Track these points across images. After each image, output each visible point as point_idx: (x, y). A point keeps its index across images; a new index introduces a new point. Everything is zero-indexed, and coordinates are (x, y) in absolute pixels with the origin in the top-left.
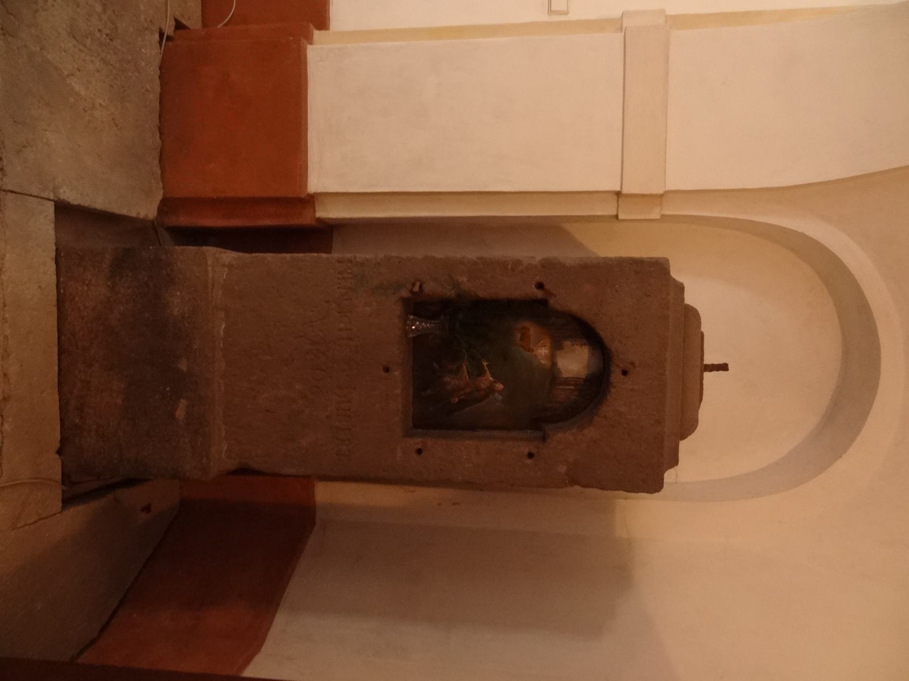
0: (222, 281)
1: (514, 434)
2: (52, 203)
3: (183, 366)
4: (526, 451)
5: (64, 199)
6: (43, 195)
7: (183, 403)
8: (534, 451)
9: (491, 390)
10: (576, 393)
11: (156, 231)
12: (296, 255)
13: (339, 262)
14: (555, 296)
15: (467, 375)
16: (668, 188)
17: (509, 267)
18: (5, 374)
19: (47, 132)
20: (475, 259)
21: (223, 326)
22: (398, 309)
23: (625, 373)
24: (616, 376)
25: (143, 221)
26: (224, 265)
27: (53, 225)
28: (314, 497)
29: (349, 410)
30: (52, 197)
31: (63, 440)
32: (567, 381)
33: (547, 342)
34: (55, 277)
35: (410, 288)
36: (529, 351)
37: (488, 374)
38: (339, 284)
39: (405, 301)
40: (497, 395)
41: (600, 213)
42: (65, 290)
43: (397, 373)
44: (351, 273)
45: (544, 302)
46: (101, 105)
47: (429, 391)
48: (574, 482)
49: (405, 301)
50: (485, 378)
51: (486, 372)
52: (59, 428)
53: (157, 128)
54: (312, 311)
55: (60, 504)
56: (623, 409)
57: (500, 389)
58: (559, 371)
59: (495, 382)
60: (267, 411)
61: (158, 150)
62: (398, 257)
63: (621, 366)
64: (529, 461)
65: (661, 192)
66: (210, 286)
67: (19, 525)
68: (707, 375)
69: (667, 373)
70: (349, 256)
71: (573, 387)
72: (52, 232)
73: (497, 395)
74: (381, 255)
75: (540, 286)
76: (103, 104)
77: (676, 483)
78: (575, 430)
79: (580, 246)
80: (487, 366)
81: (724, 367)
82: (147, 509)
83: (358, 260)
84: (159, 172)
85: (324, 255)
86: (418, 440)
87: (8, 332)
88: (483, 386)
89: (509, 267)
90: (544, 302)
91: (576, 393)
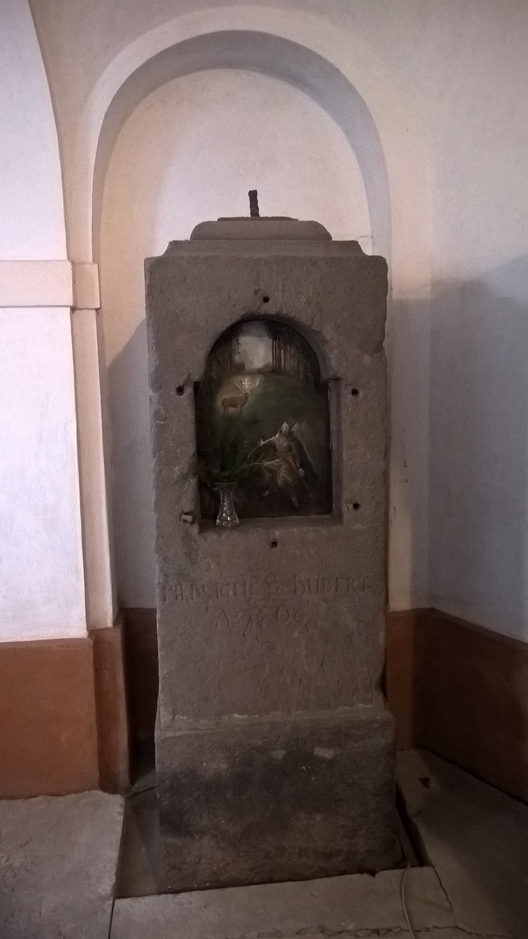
0: (191, 720)
1: (333, 409)
2: (117, 902)
3: (279, 754)
4: (350, 396)
5: (112, 890)
6: (109, 911)
7: (319, 752)
8: (350, 389)
9: (289, 435)
10: (288, 348)
11: (135, 795)
12: (159, 646)
13: (165, 600)
14: (190, 374)
15: (274, 461)
16: (65, 257)
17: (163, 423)
18: (297, 933)
19: (42, 912)
20: (155, 459)
21: (236, 716)
22: (211, 536)
23: (266, 300)
24: (270, 309)
25: (126, 808)
26: (173, 719)
27: (140, 899)
28: (405, 611)
29: (317, 580)
30: (111, 902)
31: (361, 871)
32: (277, 358)
33: (236, 379)
34: (194, 893)
35: (189, 525)
36: (246, 398)
37: (273, 439)
38: (187, 598)
39: (202, 529)
40: (294, 429)
41: (95, 327)
42: (206, 882)
43: (277, 533)
44: (176, 586)
45: (197, 386)
46: (7, 860)
47: (294, 499)
48: (379, 348)
49: (202, 529)
50: (277, 441)
51: (271, 441)
52: (348, 876)
53: (26, 801)
54: (217, 625)
55: (425, 870)
56: (303, 299)
57: (288, 426)
58: (265, 366)
59: (281, 432)
60: (322, 665)
61: (49, 798)
62: (157, 539)
63: (259, 304)
64: (361, 394)
65: (69, 264)
66: (195, 732)
67: (449, 906)
68: (263, 212)
69: (264, 256)
70: (157, 591)
71: (282, 351)
72: (148, 900)
73: (294, 429)
74: (156, 557)
75: (180, 390)
76: (5, 858)
77: (372, 237)
78: (327, 349)
79: (129, 348)
80: (264, 441)
81: (253, 195)
82: (425, 782)
83: (161, 580)
84: (73, 795)
85: (158, 616)
86: (344, 509)
87: (255, 934)
88: (286, 444)
89: (163, 423)
90: (197, 386)
91: (288, 348)
